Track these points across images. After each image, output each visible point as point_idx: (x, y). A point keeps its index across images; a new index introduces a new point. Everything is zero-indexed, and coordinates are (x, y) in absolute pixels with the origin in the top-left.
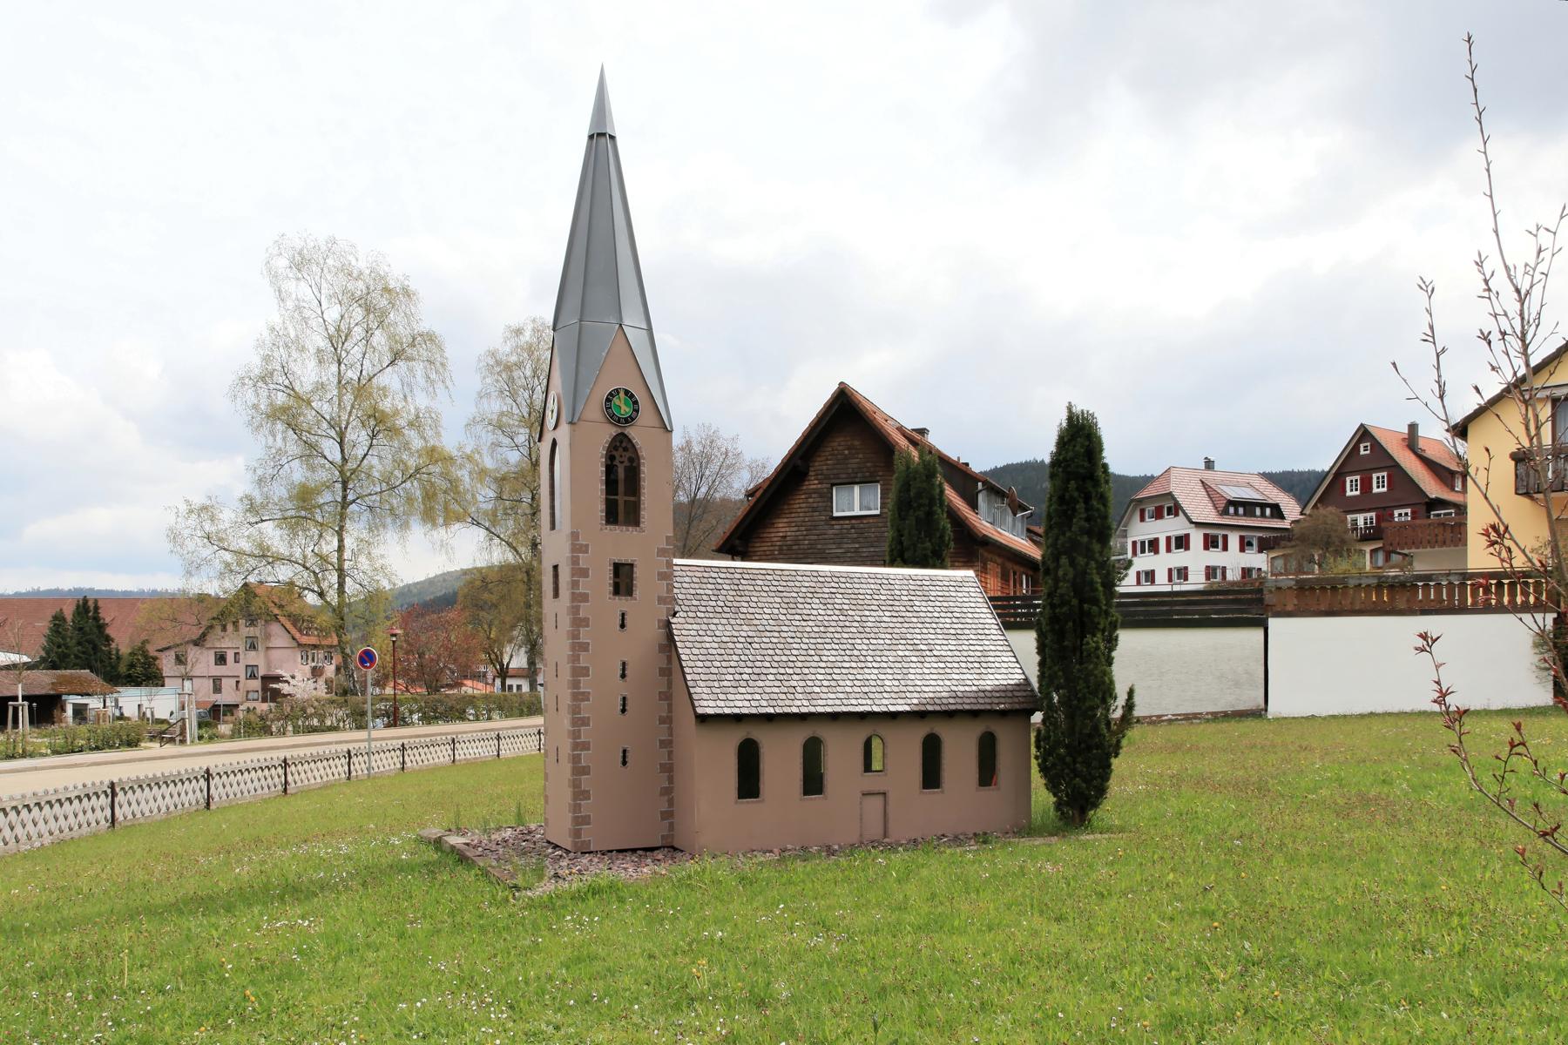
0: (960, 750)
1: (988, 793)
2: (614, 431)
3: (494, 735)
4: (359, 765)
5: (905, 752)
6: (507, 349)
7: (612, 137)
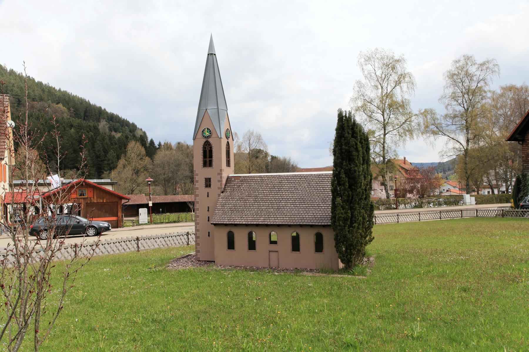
0: (307, 240)
1: (318, 255)
2: (205, 140)
3: (396, 214)
4: (401, 219)
5: (284, 238)
6: (453, 70)
7: (215, 55)
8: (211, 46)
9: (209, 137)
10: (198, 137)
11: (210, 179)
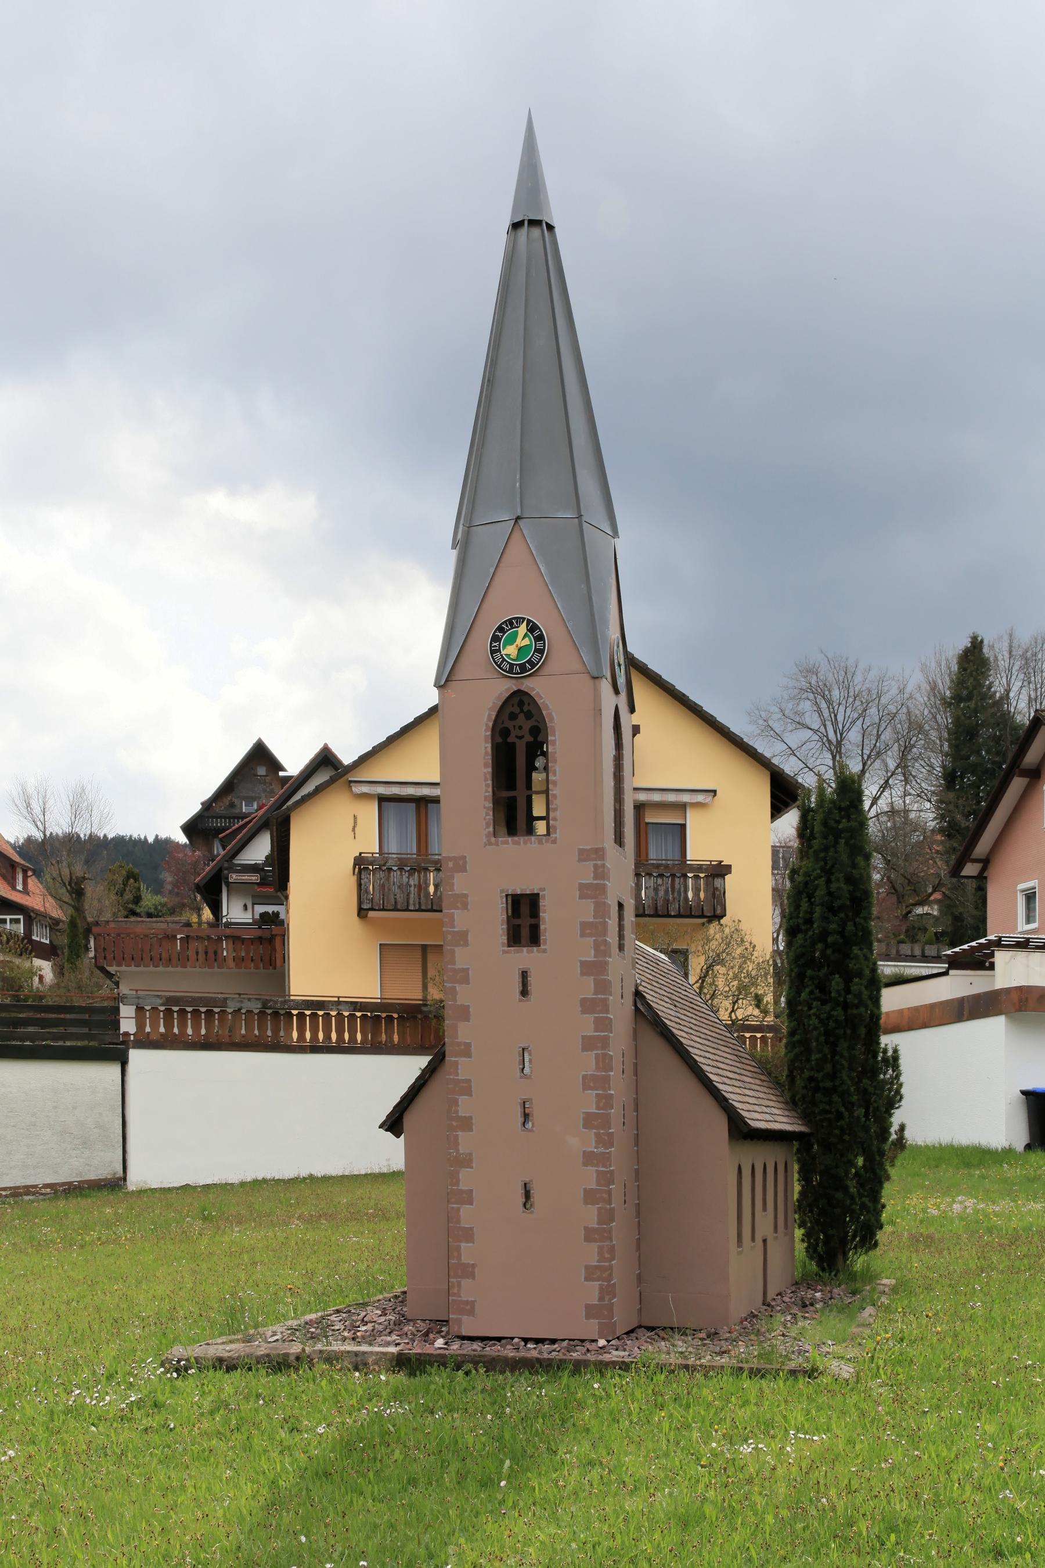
2: (504, 687)
7: (550, 228)
8: (530, 179)
9: (525, 668)
10: (465, 671)
11: (533, 900)
